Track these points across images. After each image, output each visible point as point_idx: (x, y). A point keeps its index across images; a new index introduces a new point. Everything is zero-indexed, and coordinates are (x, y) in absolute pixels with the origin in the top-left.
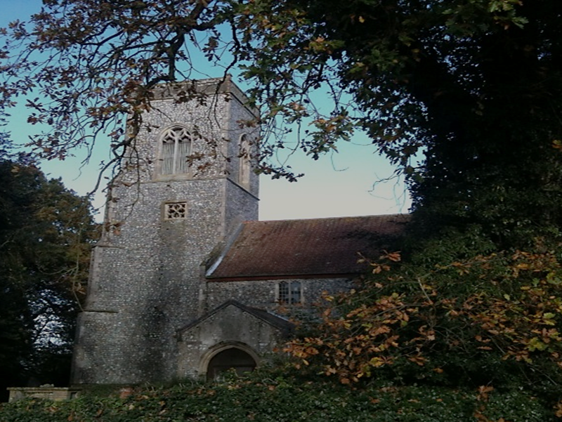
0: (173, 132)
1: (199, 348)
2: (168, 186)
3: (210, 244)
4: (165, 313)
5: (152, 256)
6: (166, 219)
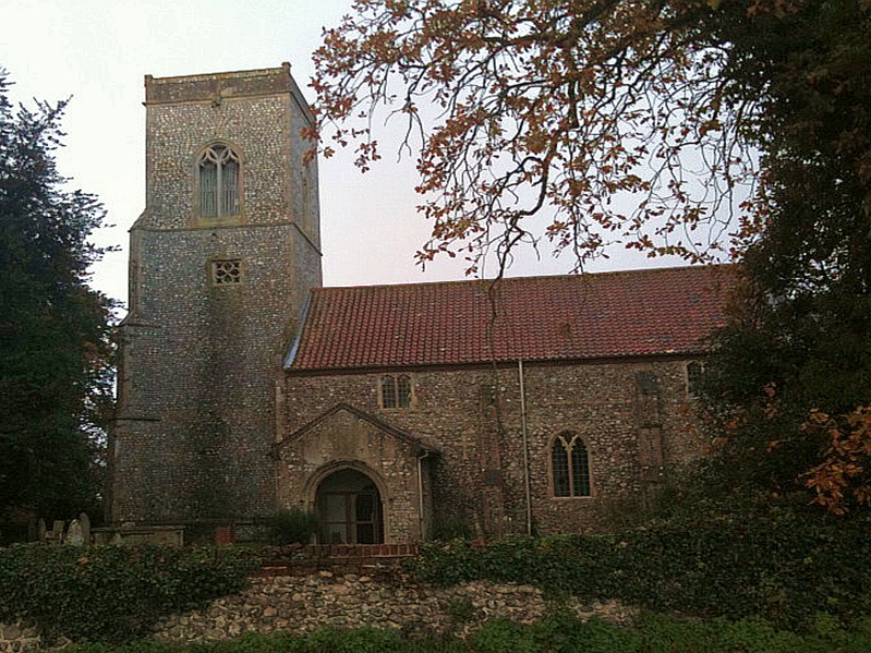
0: (213, 152)
1: (304, 468)
2: (214, 235)
3: (277, 320)
4: (224, 420)
5: (200, 339)
6: (215, 284)
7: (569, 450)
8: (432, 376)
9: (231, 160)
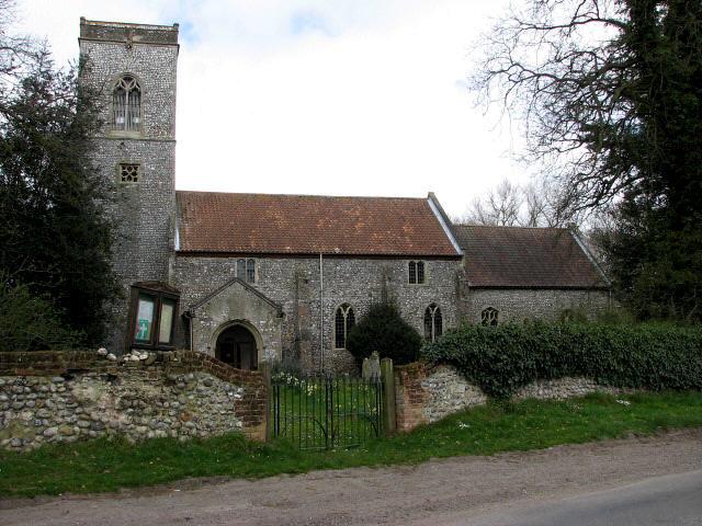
7: (345, 316)
8: (268, 260)
9: (135, 89)
